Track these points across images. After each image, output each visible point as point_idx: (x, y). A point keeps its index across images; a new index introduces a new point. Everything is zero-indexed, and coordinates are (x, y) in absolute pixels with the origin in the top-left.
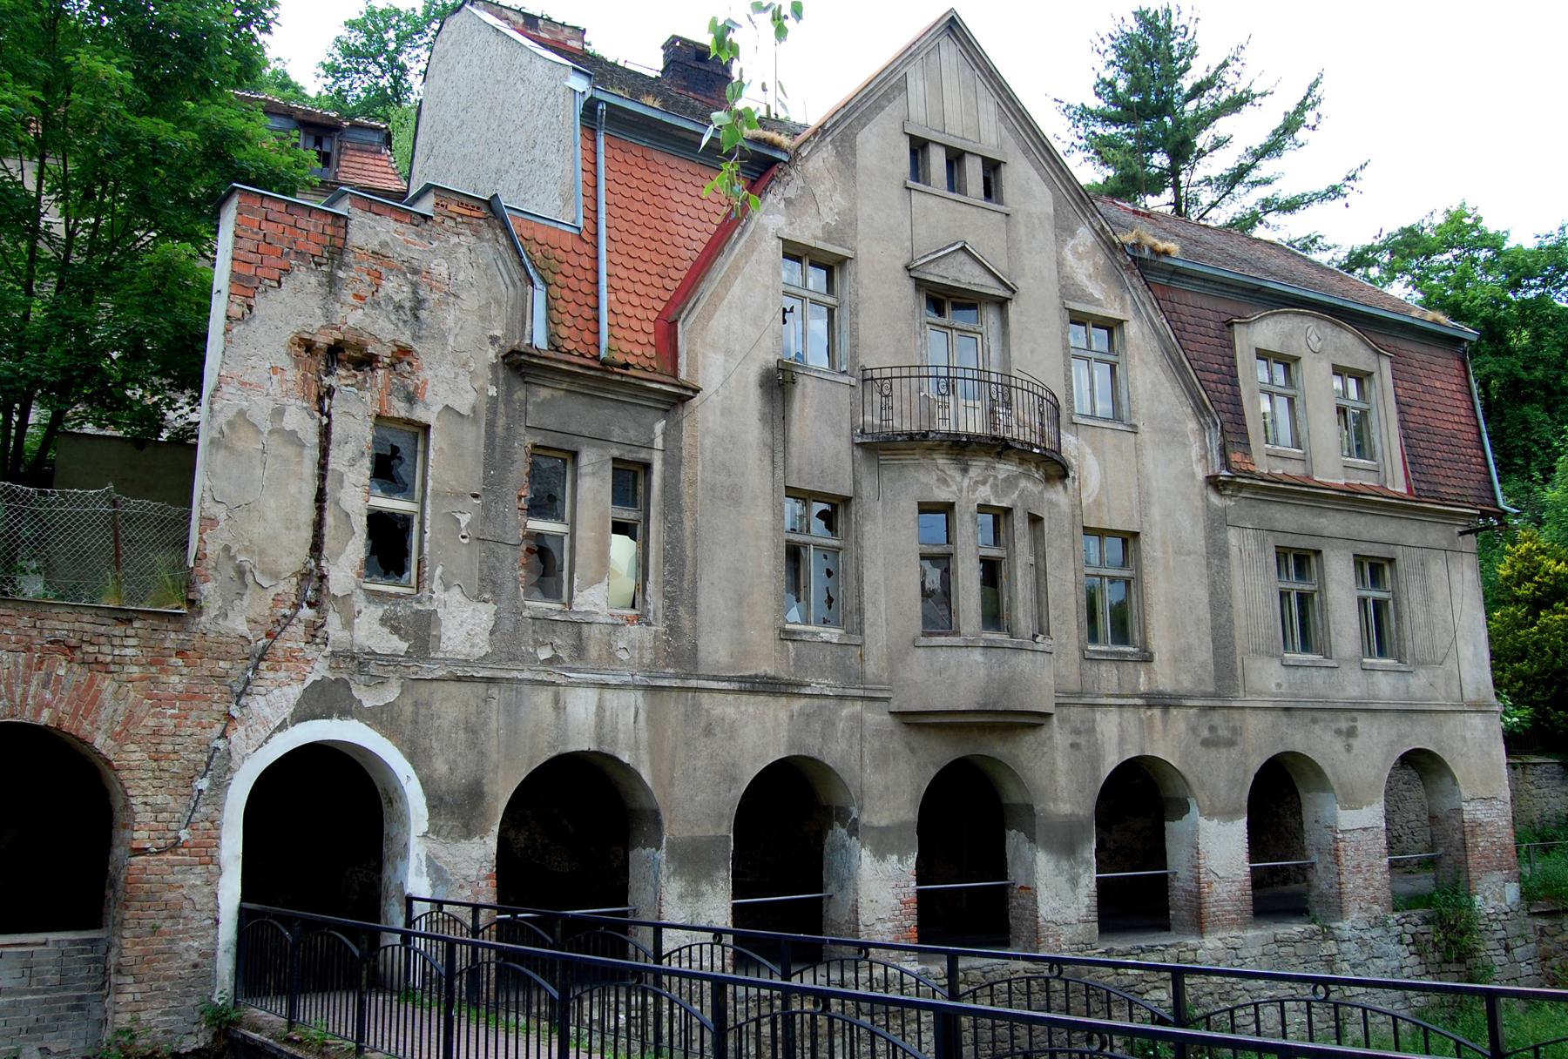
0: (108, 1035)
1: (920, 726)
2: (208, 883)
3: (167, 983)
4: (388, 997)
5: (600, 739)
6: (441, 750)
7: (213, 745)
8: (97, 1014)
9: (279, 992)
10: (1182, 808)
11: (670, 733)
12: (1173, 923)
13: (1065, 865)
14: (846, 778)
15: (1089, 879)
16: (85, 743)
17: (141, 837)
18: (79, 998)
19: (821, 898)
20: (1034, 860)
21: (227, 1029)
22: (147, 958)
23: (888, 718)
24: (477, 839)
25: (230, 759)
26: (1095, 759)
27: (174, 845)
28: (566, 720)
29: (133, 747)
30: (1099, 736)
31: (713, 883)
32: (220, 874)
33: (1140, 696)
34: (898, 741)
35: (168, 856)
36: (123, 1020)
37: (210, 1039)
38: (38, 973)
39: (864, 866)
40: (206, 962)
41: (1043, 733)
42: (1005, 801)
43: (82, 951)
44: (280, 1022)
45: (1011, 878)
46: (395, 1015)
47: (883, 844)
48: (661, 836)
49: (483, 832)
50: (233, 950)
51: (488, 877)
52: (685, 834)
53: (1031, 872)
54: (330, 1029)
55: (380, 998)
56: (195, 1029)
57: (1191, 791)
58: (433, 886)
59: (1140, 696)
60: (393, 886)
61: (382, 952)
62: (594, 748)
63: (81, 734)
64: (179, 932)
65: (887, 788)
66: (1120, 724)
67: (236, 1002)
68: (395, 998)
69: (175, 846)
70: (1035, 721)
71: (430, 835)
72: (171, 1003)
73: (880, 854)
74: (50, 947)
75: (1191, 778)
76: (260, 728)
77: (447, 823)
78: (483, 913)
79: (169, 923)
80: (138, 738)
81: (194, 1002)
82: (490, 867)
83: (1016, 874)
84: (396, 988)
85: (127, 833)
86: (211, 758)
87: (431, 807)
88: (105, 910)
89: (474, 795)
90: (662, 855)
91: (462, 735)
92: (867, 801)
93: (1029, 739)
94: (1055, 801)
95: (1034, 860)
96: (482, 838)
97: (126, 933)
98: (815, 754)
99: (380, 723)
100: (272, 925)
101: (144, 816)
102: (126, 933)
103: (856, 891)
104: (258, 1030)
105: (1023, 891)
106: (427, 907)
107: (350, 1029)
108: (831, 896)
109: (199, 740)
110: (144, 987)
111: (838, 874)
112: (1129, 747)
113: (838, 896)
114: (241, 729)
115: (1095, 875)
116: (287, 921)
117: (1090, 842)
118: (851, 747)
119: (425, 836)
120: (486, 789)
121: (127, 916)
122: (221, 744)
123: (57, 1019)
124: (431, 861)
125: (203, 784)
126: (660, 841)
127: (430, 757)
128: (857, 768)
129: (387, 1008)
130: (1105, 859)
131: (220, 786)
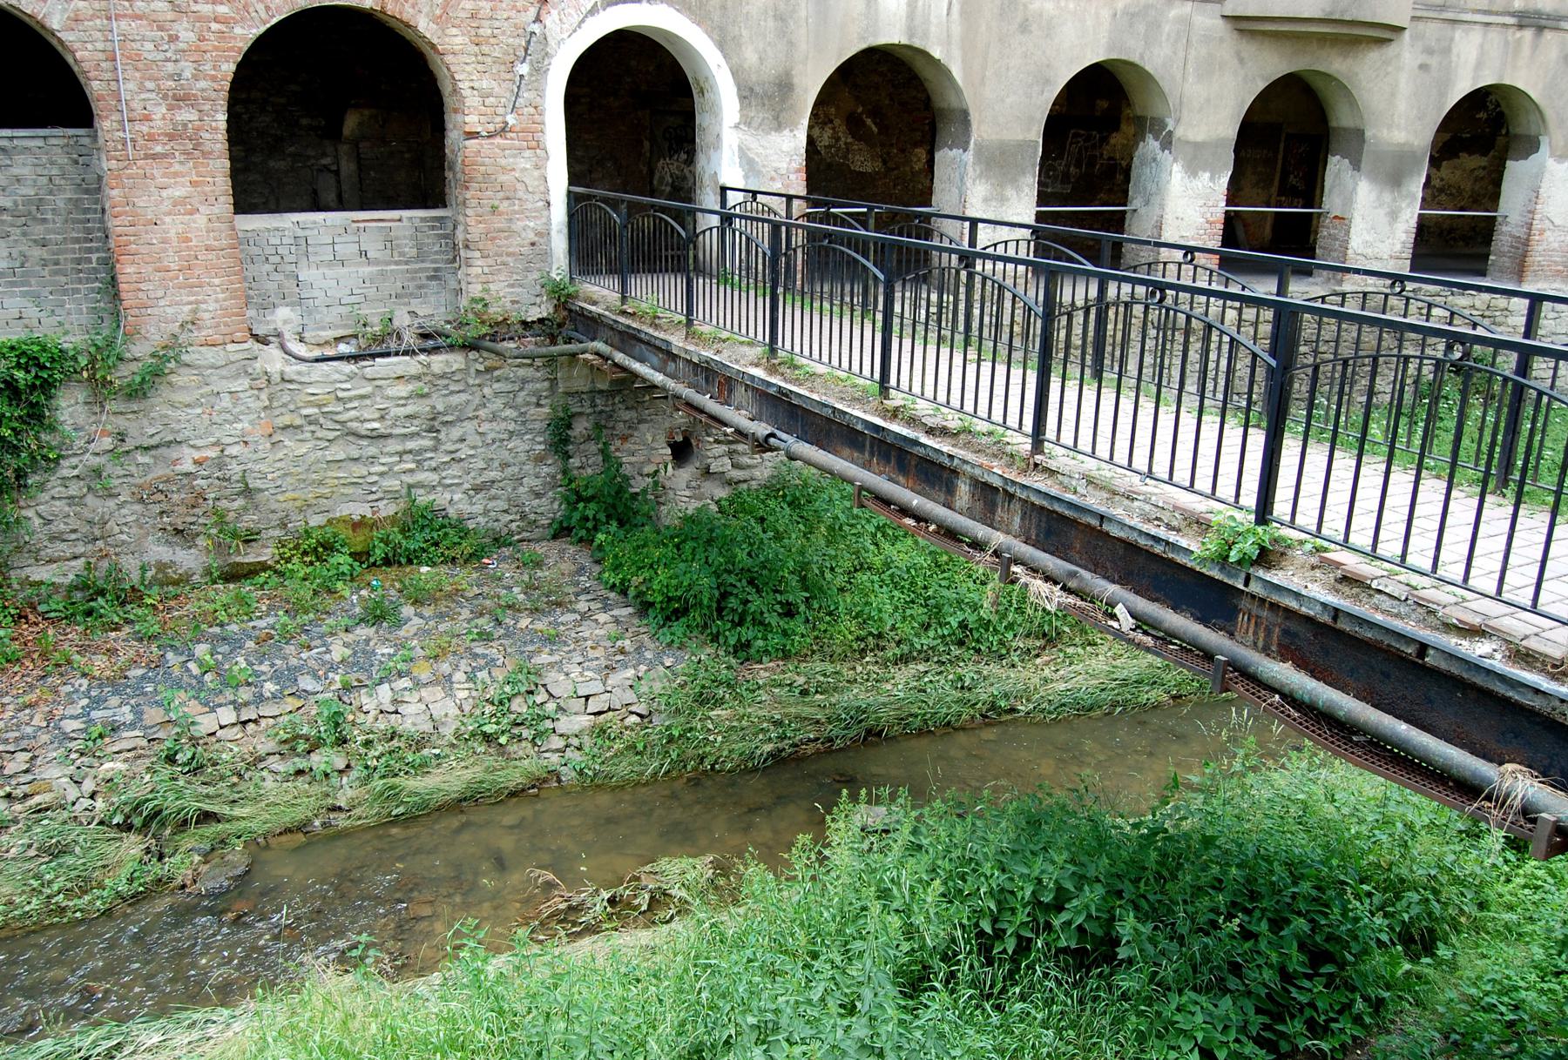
0: (464, 302)
1: (1253, 34)
2: (537, 167)
3: (509, 259)
4: (708, 281)
5: (911, 31)
6: (751, 38)
7: (529, 29)
8: (453, 284)
9: (610, 272)
10: (1530, 146)
11: (984, 28)
12: (1491, 268)
13: (1387, 197)
14: (1165, 85)
15: (1410, 214)
16: (409, 26)
17: (473, 121)
18: (436, 270)
19: (1125, 212)
20: (1354, 189)
21: (566, 302)
22: (489, 236)
23: (1221, 22)
24: (786, 132)
25: (547, 44)
26: (1444, 85)
27: (503, 130)
28: (876, 10)
29: (454, 31)
30: (1454, 59)
31: (1018, 190)
32: (548, 159)
33: (1512, 14)
34: (1228, 45)
35: (498, 140)
36: (476, 290)
37: (551, 310)
38: (397, 245)
39: (1173, 181)
40: (542, 241)
41: (1390, 50)
42: (1333, 124)
43: (433, 228)
44: (614, 297)
45: (1326, 206)
46: (714, 295)
47: (1196, 160)
48: (969, 136)
49: (793, 126)
50: (565, 231)
51: (798, 171)
52: (994, 137)
53: (1349, 201)
54: (661, 304)
55: (701, 281)
56: (538, 300)
57: (1546, 128)
58: (746, 177)
59: (1512, 14)
60: (706, 176)
61: (701, 237)
62: (904, 41)
63: (405, 17)
64: (516, 212)
65: (1208, 100)
66: (1482, 46)
67: (571, 278)
68: (714, 281)
69: (503, 130)
70: (1382, 35)
71: (742, 126)
72: (515, 277)
73: (1192, 170)
74: (405, 223)
75: (1549, 114)
76: (572, 11)
77: (758, 115)
78: (796, 203)
79: (506, 203)
80: (457, 22)
81: (536, 277)
82: (800, 160)
83: (1332, 202)
84: (715, 272)
85: (459, 118)
86: (529, 42)
87: (743, 98)
88: (447, 190)
89: (784, 87)
90: (969, 157)
91: (771, 23)
92: (1185, 113)
93: (1374, 56)
94: (1390, 127)
95: (1355, 189)
96: (791, 131)
97: (469, 212)
98: (1135, 59)
99: (690, 9)
100: (600, 207)
101: (472, 101)
102: (469, 212)
103: (1162, 207)
104: (595, 303)
105: (1337, 221)
106: (740, 197)
107: (681, 306)
108: (1135, 211)
109: (516, 25)
110: (490, 261)
111: (1145, 189)
112: (1487, 72)
113: (1142, 211)
114: (554, 12)
115: (1418, 211)
116: (614, 204)
117: (1420, 175)
118: (1175, 53)
119: (737, 127)
120: (796, 81)
121: (468, 196)
122: (536, 28)
123: (420, 287)
124: (743, 152)
125: (524, 69)
126: (968, 143)
127: (739, 45)
128: (1179, 76)
129: (708, 290)
130: (1433, 193)
131: (540, 71)
